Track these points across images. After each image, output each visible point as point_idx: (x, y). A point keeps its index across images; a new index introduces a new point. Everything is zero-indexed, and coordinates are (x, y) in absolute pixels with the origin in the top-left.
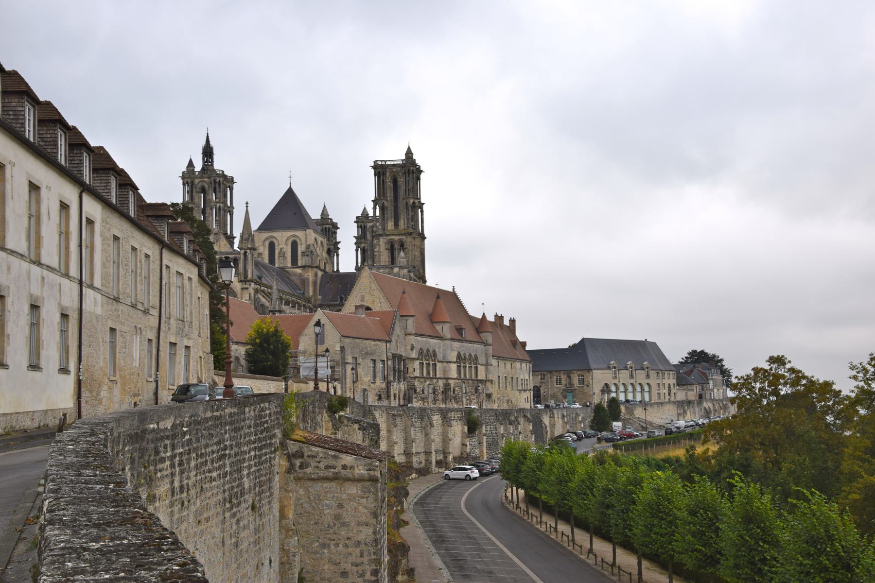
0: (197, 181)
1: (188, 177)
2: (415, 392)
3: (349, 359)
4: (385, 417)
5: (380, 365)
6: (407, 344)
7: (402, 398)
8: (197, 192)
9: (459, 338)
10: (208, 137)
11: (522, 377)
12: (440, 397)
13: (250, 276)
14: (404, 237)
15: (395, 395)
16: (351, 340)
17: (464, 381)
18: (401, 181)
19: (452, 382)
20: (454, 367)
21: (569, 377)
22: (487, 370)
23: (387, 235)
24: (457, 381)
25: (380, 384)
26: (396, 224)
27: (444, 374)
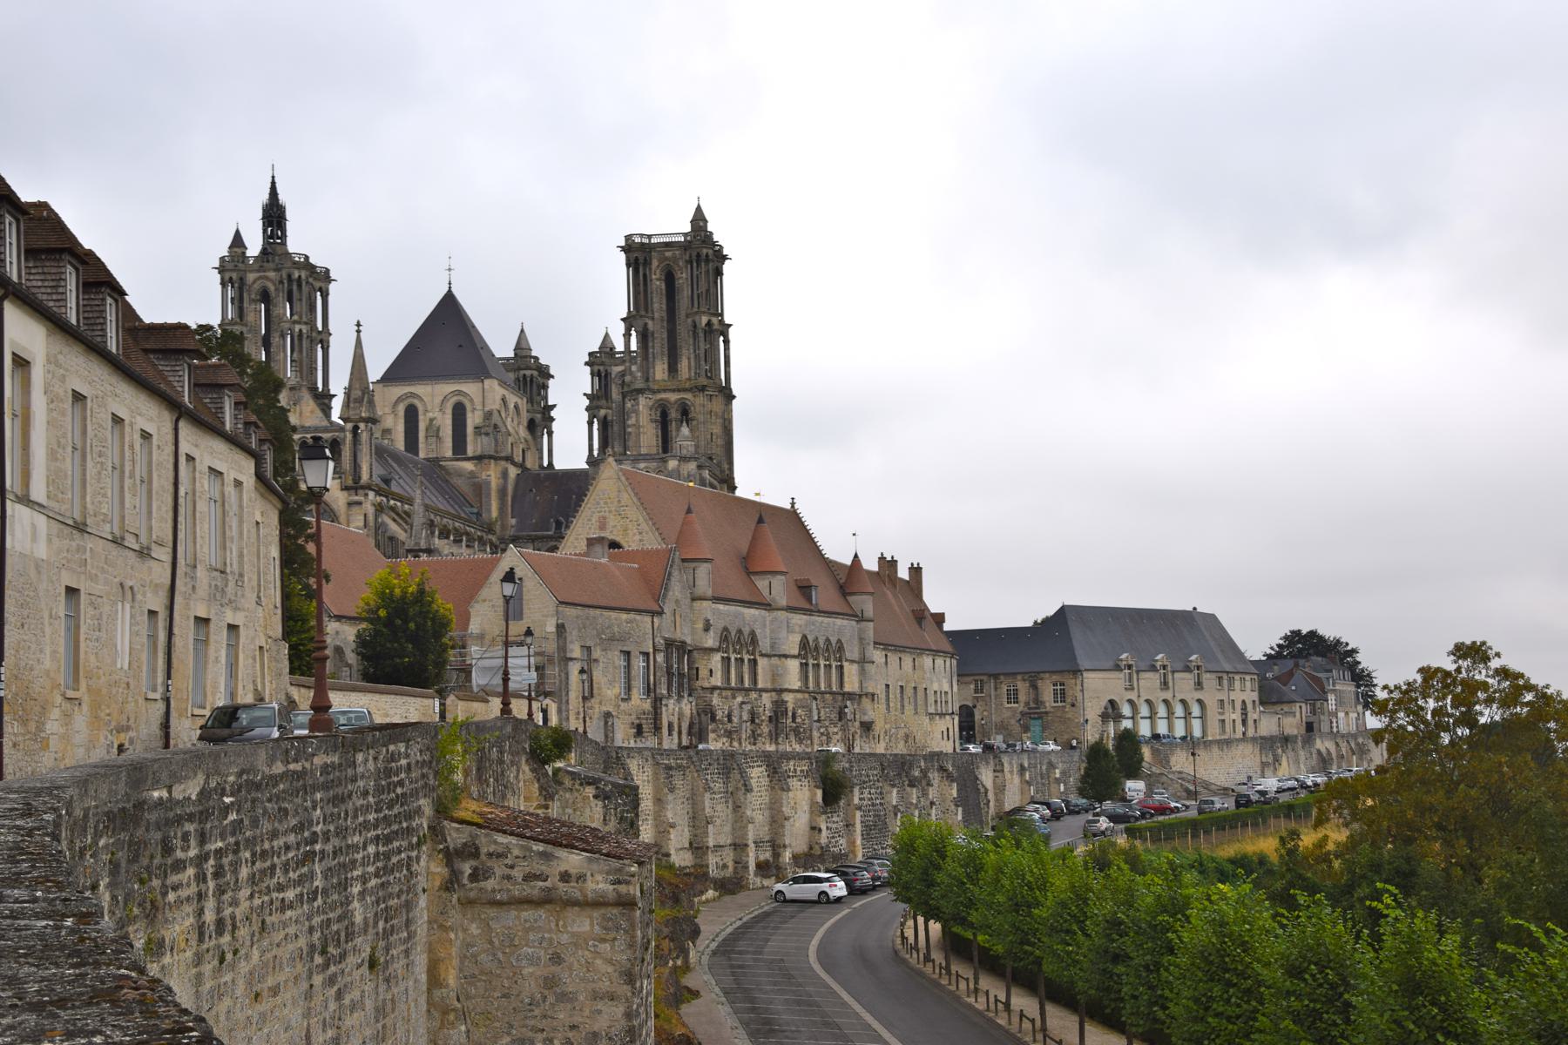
0: (251, 277)
1: (233, 268)
2: (713, 719)
4: (649, 770)
5: (639, 663)
6: (695, 619)
7: (684, 732)
8: (254, 301)
10: (273, 183)
11: (936, 687)
12: (765, 729)
13: (365, 477)
14: (688, 396)
18: (682, 277)
19: (789, 697)
20: (793, 666)
21: (1035, 687)
22: (862, 672)
23: (654, 392)
24: (799, 696)
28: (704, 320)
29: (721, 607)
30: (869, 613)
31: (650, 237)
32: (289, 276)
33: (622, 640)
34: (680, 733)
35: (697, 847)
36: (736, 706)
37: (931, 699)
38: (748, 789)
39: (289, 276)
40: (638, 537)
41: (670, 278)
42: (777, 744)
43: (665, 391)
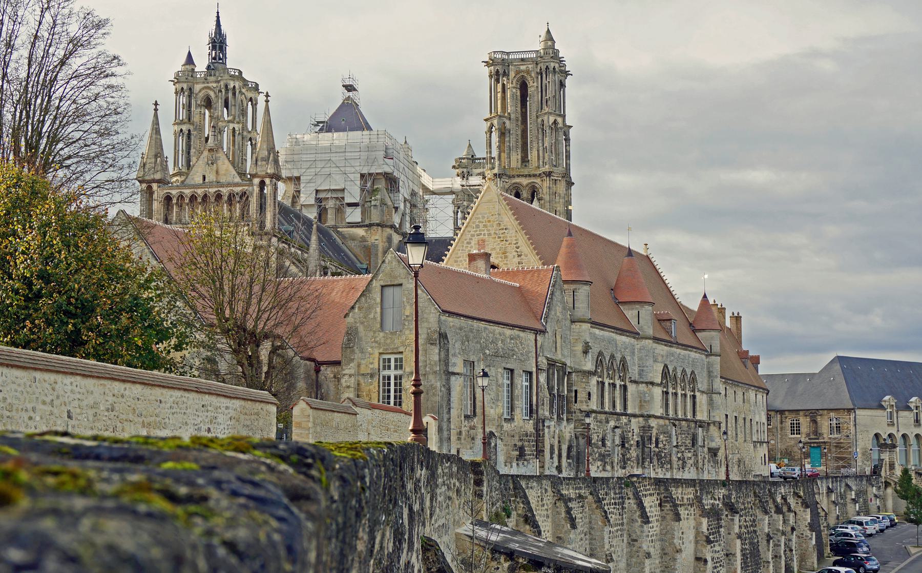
0: (197, 88)
1: (186, 80)
2: (589, 442)
3: (458, 365)
4: (549, 499)
5: (522, 382)
6: (574, 343)
7: (564, 454)
8: (200, 106)
9: (668, 338)
10: (218, 17)
11: (757, 419)
12: (633, 453)
13: (268, 225)
14: (538, 181)
15: (552, 447)
16: (462, 322)
17: (675, 422)
18: (533, 87)
19: (653, 423)
20: (658, 391)
21: (814, 422)
22: (711, 403)
23: (510, 177)
24: (661, 422)
25: (523, 423)
26: (525, 160)
27: (641, 407)
28: (552, 119)
29: (597, 331)
30: (717, 349)
31: (508, 54)
32: (226, 86)
33: (505, 357)
34: (560, 456)
35: (255, 326)
36: (609, 431)
37: (755, 429)
38: (646, 519)
39: (226, 86)
40: (517, 260)
41: (524, 87)
42: (644, 468)
43: (518, 176)
